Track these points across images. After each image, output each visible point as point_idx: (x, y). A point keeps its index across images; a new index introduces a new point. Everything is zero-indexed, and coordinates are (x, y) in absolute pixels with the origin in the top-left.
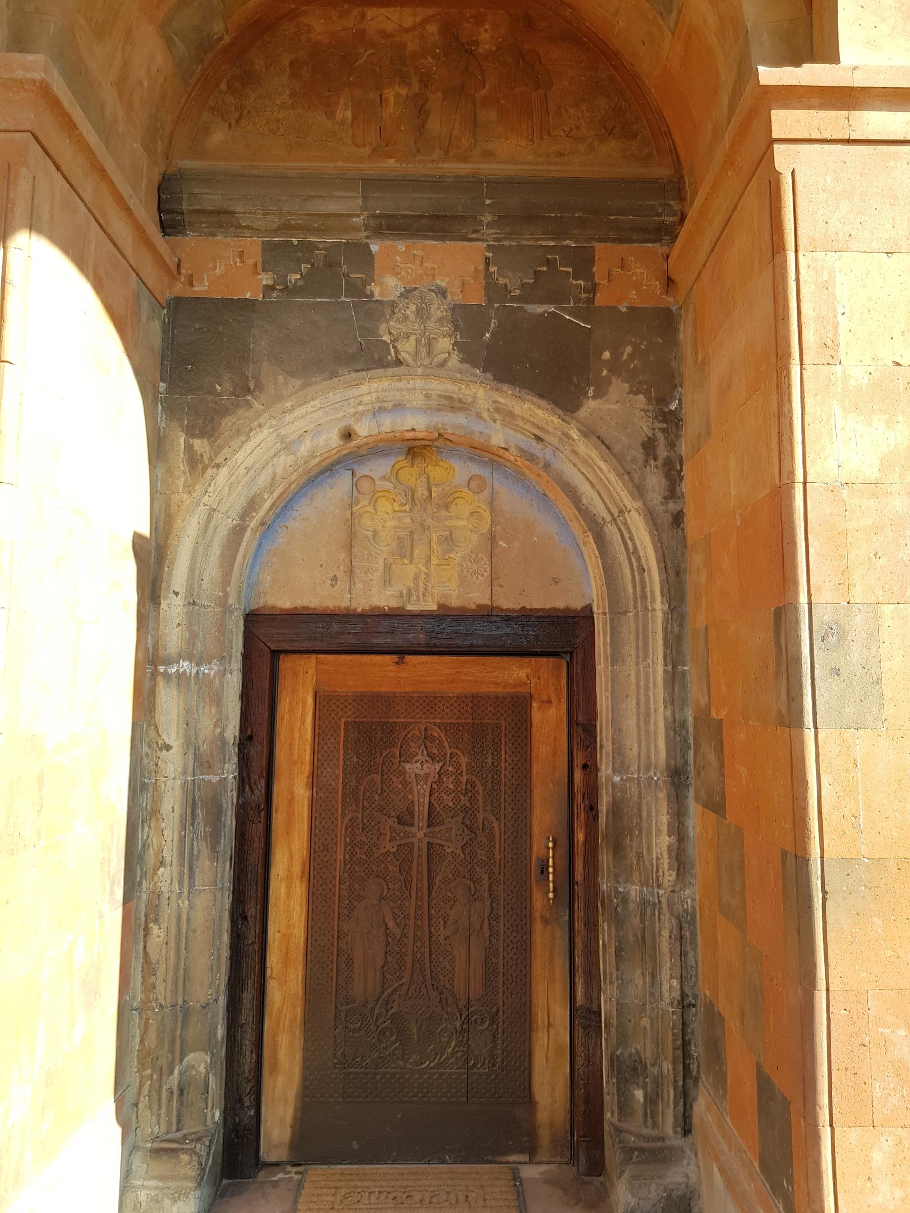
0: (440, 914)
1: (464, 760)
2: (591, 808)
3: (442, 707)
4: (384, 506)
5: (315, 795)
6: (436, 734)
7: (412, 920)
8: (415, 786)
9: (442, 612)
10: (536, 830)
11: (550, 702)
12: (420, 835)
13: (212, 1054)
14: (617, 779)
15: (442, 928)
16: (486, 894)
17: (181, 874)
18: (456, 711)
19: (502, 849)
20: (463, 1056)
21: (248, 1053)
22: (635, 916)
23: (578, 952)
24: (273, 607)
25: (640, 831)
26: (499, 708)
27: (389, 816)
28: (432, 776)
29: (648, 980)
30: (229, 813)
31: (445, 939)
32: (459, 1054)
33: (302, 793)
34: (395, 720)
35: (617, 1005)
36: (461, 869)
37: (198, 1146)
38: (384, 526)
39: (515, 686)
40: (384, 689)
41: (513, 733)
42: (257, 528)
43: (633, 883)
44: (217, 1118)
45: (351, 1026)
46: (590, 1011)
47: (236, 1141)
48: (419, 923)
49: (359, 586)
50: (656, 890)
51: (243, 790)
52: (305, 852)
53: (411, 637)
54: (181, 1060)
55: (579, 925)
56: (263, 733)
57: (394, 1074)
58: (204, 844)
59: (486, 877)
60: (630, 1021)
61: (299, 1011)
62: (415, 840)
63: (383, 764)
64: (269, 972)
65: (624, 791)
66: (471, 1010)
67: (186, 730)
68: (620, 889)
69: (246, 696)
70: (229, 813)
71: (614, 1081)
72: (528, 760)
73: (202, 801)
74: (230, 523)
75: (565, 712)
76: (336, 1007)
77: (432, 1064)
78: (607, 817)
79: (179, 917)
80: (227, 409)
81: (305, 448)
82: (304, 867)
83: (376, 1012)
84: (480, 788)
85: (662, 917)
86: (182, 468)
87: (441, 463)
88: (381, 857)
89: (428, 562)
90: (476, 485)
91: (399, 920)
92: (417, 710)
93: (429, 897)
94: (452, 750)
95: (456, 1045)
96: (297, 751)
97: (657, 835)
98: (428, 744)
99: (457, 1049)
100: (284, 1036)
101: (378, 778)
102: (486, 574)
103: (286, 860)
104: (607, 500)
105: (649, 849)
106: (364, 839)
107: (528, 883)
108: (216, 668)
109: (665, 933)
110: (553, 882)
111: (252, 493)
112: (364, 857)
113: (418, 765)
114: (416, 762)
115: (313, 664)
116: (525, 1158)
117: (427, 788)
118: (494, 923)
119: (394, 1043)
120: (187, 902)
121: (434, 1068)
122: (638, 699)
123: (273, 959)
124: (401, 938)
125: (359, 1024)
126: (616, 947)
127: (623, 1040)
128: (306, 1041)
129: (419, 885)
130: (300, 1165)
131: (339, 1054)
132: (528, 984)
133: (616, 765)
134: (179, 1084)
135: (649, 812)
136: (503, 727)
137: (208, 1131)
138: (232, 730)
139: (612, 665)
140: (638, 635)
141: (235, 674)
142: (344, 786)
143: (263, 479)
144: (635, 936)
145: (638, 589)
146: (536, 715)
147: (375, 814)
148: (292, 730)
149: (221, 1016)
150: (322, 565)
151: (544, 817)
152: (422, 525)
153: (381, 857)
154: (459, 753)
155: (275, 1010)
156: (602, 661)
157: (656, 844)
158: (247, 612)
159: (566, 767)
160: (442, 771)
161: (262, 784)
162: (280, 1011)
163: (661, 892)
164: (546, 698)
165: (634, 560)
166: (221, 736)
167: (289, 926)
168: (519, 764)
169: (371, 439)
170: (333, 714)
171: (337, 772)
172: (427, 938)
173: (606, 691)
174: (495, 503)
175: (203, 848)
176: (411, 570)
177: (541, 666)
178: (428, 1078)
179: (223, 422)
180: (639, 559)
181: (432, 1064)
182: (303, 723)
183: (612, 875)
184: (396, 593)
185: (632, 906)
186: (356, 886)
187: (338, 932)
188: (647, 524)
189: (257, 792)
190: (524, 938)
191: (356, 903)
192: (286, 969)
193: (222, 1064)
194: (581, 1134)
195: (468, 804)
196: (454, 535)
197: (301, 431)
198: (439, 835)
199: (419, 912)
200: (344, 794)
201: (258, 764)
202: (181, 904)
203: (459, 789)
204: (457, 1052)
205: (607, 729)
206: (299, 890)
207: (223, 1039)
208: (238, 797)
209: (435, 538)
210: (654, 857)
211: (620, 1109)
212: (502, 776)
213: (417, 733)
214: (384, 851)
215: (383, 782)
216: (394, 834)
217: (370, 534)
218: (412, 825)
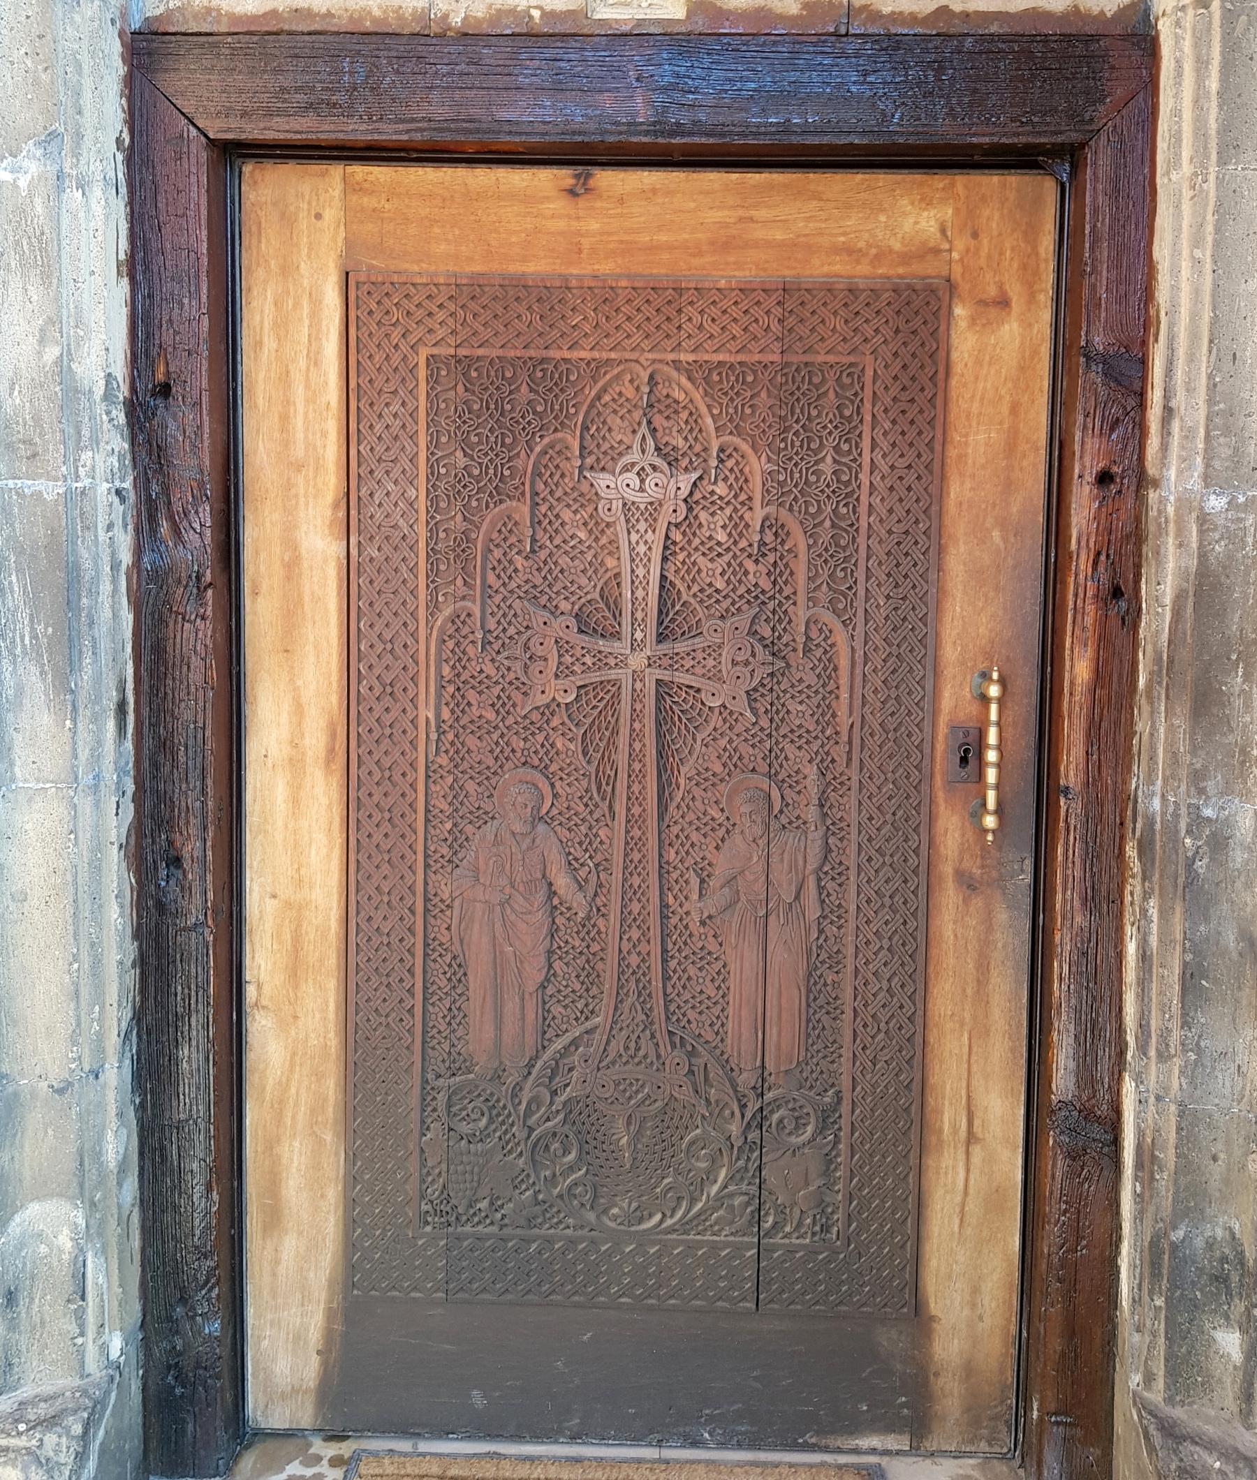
0: (689, 861)
1: (757, 466)
2: (1117, 593)
3: (697, 319)
5: (354, 552)
6: (677, 394)
7: (618, 875)
8: (623, 537)
9: (700, 25)
10: (950, 653)
11: (1003, 302)
12: (637, 661)
13: (93, 1204)
14: (1216, 503)
15: (695, 897)
16: (812, 814)
18: (736, 330)
19: (858, 702)
20: (748, 1204)
21: (199, 1190)
23: (1060, 968)
26: (859, 321)
27: (555, 612)
28: (668, 507)
30: (106, 587)
31: (703, 923)
32: (737, 1201)
33: (321, 548)
34: (567, 355)
35: (1181, 1115)
36: (746, 749)
37: (51, 1439)
39: (905, 258)
40: (536, 267)
41: (894, 391)
44: (115, 1353)
45: (464, 1128)
46: (1087, 1114)
47: (178, 1391)
48: (636, 881)
51: (154, 531)
52: (334, 699)
53: (607, 102)
55: (1066, 899)
56: (197, 377)
57: (572, 1242)
58: (34, 669)
59: (812, 771)
60: (1215, 1159)
61: (331, 1087)
62: (623, 675)
63: (537, 474)
64: (251, 992)
65: (1235, 537)
66: (769, 1096)
68: (1208, 812)
69: (141, 264)
70: (106, 587)
71: (1160, 1302)
72: (936, 466)
73: (20, 552)
75: (1047, 332)
76: (425, 1081)
77: (669, 1222)
78: (1177, 614)
82: (333, 736)
83: (526, 1096)
84: (799, 540)
88: (535, 716)
91: (583, 873)
92: (628, 326)
93: (661, 817)
94: (727, 438)
95: (730, 1179)
96: (300, 436)
98: (658, 421)
99: (731, 1188)
100: (296, 1144)
101: (523, 511)
103: (284, 719)
106: (489, 669)
107: (924, 787)
108: (33, 168)
110: (998, 787)
112: (490, 715)
113: (632, 478)
114: (626, 469)
115: (337, 191)
116: (903, 1443)
117: (657, 540)
118: (831, 886)
119: (572, 1169)
121: (671, 1230)
123: (263, 963)
124: (589, 918)
125: (484, 1121)
126: (1185, 965)
127: (1191, 1202)
128: (352, 1157)
129: (636, 788)
130: (344, 1438)
131: (434, 1191)
132: (918, 1039)
133: (1217, 464)
136: (869, 373)
137: (85, 1392)
138: (103, 351)
139: (1222, 162)
141: (97, 192)
142: (433, 530)
146: (963, 339)
147: (517, 605)
148: (285, 378)
149: (112, 1110)
151: (977, 617)
153: (535, 716)
154: (745, 447)
155: (271, 1082)
156: (1186, 154)
158: (135, 25)
159: (1041, 487)
160: (697, 496)
161: (205, 515)
162: (284, 1086)
164: (992, 291)
166: (63, 369)
167: (299, 883)
168: (911, 478)
170: (396, 337)
171: (412, 493)
172: (654, 922)
173: (1197, 242)
177: (983, 199)
178: (659, 1255)
181: (669, 1222)
182: (315, 360)
183: (1183, 773)
186: (471, 786)
187: (427, 900)
189: (191, 537)
190: (912, 925)
191: (469, 829)
192: (296, 987)
193: (125, 1222)
194: (1052, 1407)
195: (765, 584)
198: (688, 663)
199: (636, 856)
200: (432, 551)
201: (193, 462)
203: (743, 543)
204: (731, 1195)
205: (1191, 358)
206: (323, 797)
207: (122, 1169)
208: (138, 552)
211: (1173, 1372)
212: (863, 509)
213: (629, 392)
214: (541, 700)
215: (536, 523)
216: (568, 659)
218: (616, 636)
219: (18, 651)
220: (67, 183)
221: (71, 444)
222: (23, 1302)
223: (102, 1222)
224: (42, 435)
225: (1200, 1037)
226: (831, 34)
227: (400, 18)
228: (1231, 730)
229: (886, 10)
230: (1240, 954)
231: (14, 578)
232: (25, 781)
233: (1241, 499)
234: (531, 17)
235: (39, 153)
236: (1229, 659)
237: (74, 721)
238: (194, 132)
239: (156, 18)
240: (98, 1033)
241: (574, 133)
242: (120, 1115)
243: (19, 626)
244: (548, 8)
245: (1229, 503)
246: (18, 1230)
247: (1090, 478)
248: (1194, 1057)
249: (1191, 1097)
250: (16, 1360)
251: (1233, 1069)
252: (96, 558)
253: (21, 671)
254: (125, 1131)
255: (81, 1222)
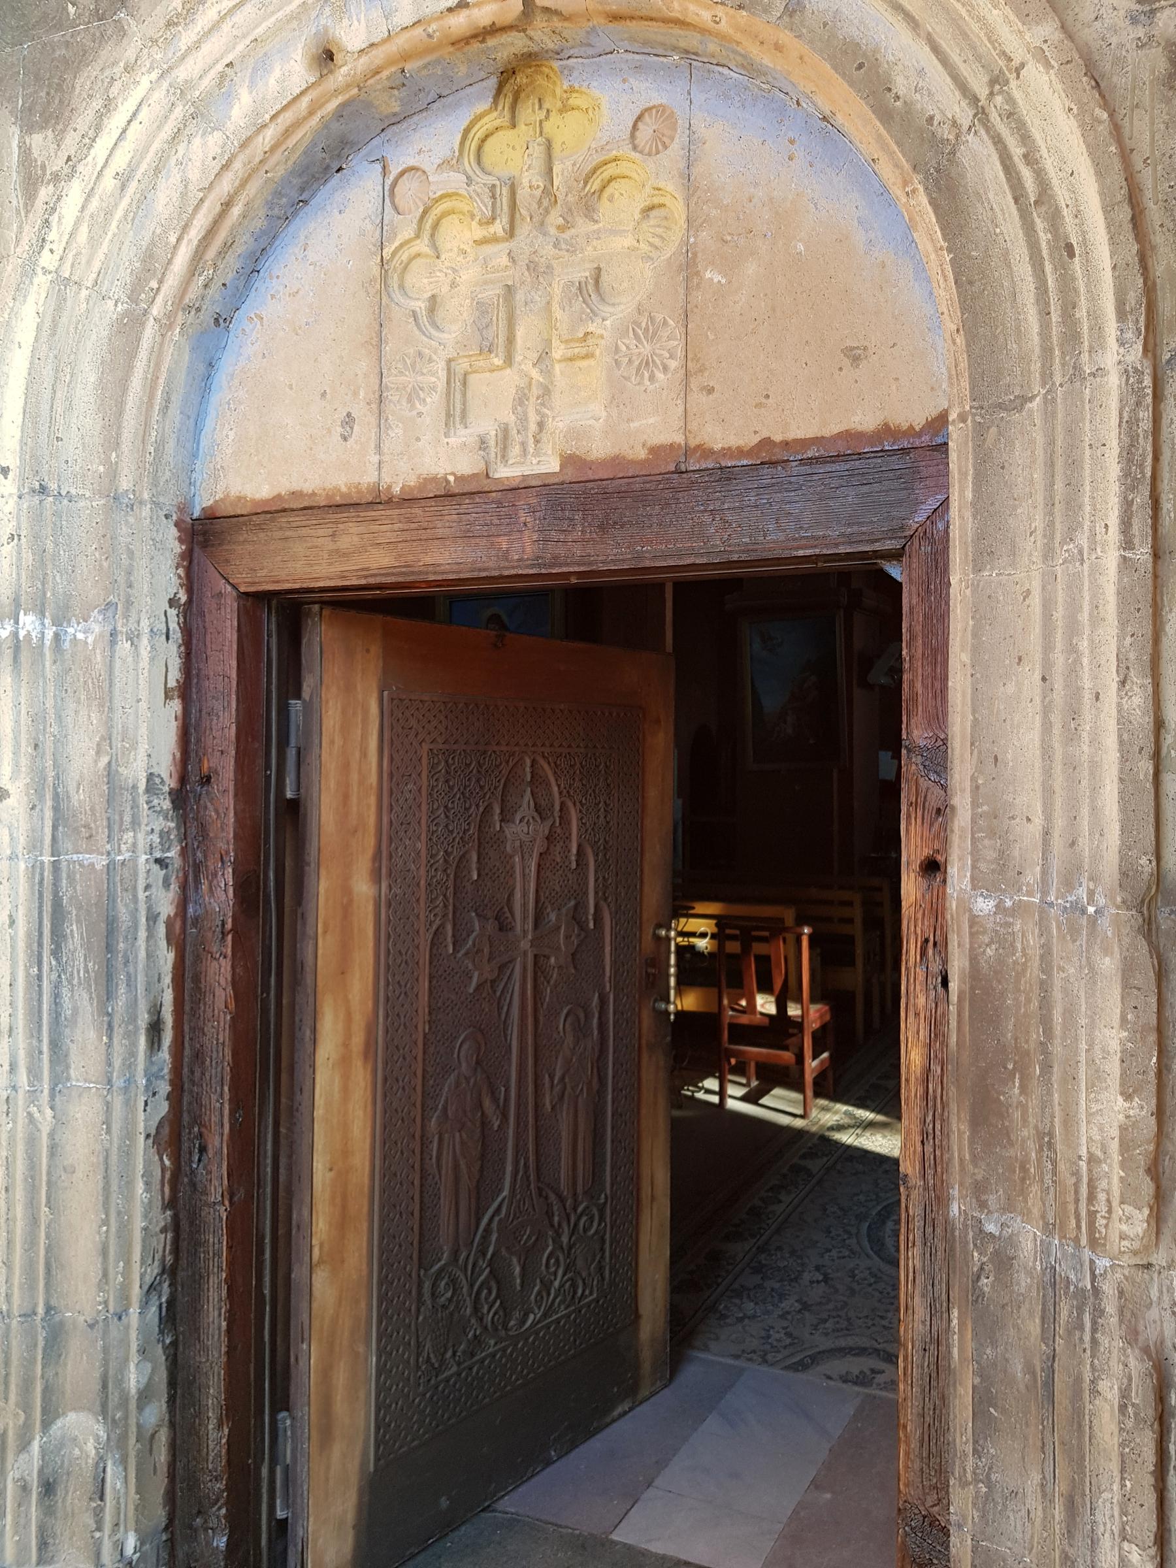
4: (458, 235)
17: (34, 1055)
22: (1031, 1314)
24: (239, 498)
25: (1047, 1067)
29: (1058, 1512)
38: (453, 285)
42: (171, 316)
43: (1027, 1215)
49: (397, 432)
50: (1087, 1254)
54: (46, 1425)
58: (86, 996)
65: (1005, 942)
67: (34, 758)
68: (991, 1228)
73: (79, 908)
74: (111, 310)
79: (32, 1142)
80: (85, 52)
81: (240, 110)
85: (1104, 1341)
86: (15, 202)
87: (574, 101)
89: (543, 357)
90: (649, 129)
96: (355, 809)
97: (1090, 1087)
102: (673, 364)
104: (955, 58)
105: (1069, 1121)
108: (97, 628)
109: (1110, 1390)
111: (147, 236)
120: (49, 1112)
122: (1047, 664)
133: (983, 866)
134: (41, 1471)
135: (1070, 1013)
140: (1051, 465)
143: (165, 199)
144: (1029, 1369)
145: (1055, 317)
150: (324, 394)
152: (532, 266)
157: (1089, 1115)
163: (1103, 1263)
165: (1040, 225)
169: (378, 56)
174: (695, 171)
175: (82, 1003)
176: (509, 380)
179: (78, 82)
180: (1055, 220)
182: (364, 754)
184: (472, 441)
185: (1023, 1282)
188: (1071, 90)
196: (604, 277)
197: (220, 67)
202: (37, 1115)
209: (557, 290)
210: (1083, 1152)
217: (420, 306)
219: (75, 982)
220: (119, 638)
221: (116, 828)
222: (60, 1492)
223: (124, 1437)
224: (95, 822)
225: (990, 1468)
226: (673, 473)
227: (359, 492)
228: (1012, 1145)
229: (717, 447)
230: (1027, 1387)
231: (74, 927)
232: (78, 1080)
233: (1009, 903)
234: (448, 482)
235: (101, 618)
236: (1006, 1068)
237: (110, 1038)
238: (229, 588)
239: (211, 507)
240: (122, 1284)
241: (480, 570)
242: (142, 1351)
243: (77, 963)
244: (459, 474)
245: (997, 906)
246: (59, 1433)
247: (916, 866)
248: (984, 1490)
249: (983, 1533)
250: (51, 1541)
251: (1024, 1513)
252: (134, 914)
253: (77, 997)
254: (149, 1365)
255: (103, 1434)
